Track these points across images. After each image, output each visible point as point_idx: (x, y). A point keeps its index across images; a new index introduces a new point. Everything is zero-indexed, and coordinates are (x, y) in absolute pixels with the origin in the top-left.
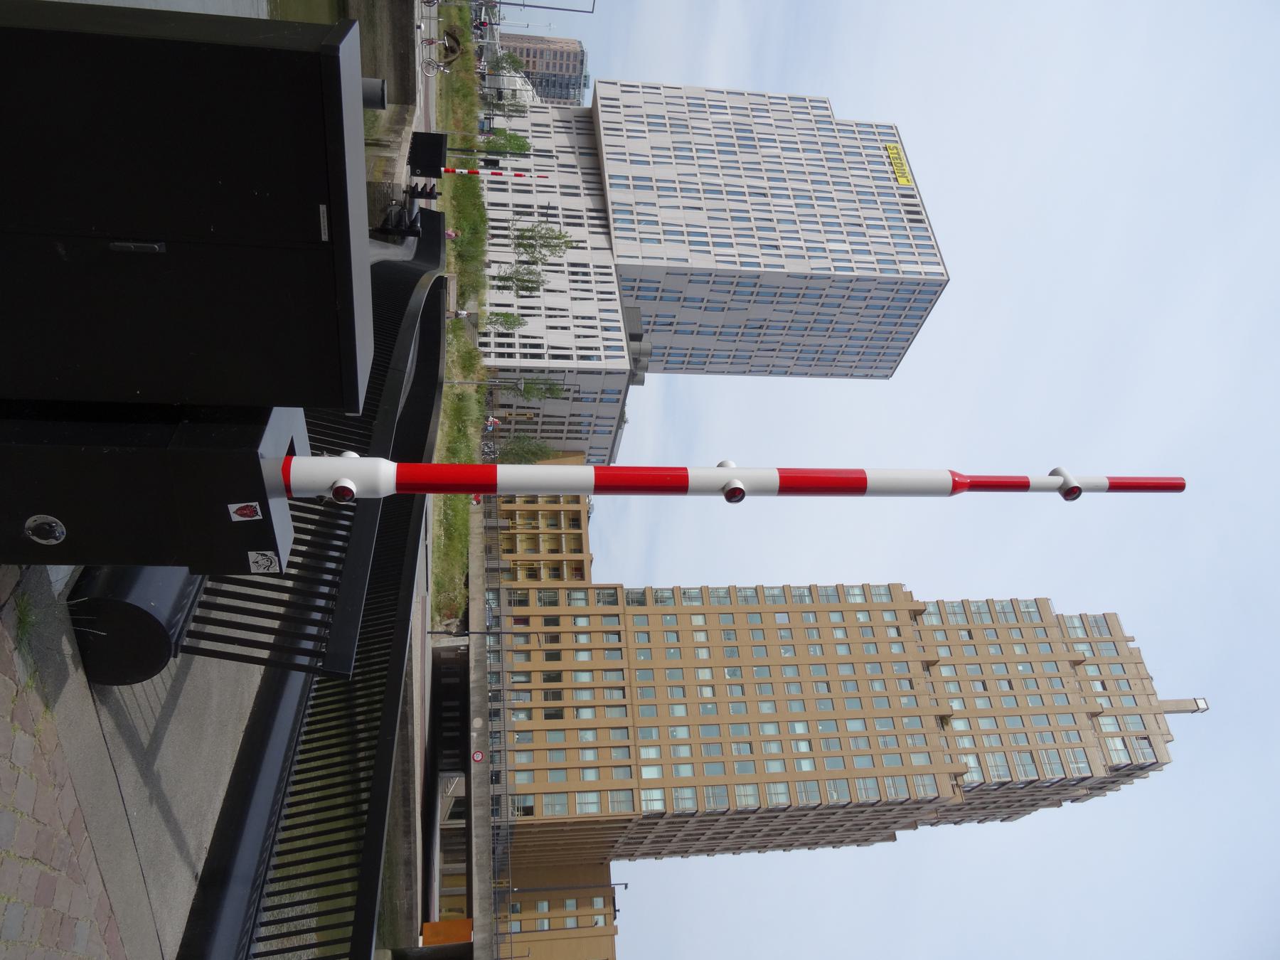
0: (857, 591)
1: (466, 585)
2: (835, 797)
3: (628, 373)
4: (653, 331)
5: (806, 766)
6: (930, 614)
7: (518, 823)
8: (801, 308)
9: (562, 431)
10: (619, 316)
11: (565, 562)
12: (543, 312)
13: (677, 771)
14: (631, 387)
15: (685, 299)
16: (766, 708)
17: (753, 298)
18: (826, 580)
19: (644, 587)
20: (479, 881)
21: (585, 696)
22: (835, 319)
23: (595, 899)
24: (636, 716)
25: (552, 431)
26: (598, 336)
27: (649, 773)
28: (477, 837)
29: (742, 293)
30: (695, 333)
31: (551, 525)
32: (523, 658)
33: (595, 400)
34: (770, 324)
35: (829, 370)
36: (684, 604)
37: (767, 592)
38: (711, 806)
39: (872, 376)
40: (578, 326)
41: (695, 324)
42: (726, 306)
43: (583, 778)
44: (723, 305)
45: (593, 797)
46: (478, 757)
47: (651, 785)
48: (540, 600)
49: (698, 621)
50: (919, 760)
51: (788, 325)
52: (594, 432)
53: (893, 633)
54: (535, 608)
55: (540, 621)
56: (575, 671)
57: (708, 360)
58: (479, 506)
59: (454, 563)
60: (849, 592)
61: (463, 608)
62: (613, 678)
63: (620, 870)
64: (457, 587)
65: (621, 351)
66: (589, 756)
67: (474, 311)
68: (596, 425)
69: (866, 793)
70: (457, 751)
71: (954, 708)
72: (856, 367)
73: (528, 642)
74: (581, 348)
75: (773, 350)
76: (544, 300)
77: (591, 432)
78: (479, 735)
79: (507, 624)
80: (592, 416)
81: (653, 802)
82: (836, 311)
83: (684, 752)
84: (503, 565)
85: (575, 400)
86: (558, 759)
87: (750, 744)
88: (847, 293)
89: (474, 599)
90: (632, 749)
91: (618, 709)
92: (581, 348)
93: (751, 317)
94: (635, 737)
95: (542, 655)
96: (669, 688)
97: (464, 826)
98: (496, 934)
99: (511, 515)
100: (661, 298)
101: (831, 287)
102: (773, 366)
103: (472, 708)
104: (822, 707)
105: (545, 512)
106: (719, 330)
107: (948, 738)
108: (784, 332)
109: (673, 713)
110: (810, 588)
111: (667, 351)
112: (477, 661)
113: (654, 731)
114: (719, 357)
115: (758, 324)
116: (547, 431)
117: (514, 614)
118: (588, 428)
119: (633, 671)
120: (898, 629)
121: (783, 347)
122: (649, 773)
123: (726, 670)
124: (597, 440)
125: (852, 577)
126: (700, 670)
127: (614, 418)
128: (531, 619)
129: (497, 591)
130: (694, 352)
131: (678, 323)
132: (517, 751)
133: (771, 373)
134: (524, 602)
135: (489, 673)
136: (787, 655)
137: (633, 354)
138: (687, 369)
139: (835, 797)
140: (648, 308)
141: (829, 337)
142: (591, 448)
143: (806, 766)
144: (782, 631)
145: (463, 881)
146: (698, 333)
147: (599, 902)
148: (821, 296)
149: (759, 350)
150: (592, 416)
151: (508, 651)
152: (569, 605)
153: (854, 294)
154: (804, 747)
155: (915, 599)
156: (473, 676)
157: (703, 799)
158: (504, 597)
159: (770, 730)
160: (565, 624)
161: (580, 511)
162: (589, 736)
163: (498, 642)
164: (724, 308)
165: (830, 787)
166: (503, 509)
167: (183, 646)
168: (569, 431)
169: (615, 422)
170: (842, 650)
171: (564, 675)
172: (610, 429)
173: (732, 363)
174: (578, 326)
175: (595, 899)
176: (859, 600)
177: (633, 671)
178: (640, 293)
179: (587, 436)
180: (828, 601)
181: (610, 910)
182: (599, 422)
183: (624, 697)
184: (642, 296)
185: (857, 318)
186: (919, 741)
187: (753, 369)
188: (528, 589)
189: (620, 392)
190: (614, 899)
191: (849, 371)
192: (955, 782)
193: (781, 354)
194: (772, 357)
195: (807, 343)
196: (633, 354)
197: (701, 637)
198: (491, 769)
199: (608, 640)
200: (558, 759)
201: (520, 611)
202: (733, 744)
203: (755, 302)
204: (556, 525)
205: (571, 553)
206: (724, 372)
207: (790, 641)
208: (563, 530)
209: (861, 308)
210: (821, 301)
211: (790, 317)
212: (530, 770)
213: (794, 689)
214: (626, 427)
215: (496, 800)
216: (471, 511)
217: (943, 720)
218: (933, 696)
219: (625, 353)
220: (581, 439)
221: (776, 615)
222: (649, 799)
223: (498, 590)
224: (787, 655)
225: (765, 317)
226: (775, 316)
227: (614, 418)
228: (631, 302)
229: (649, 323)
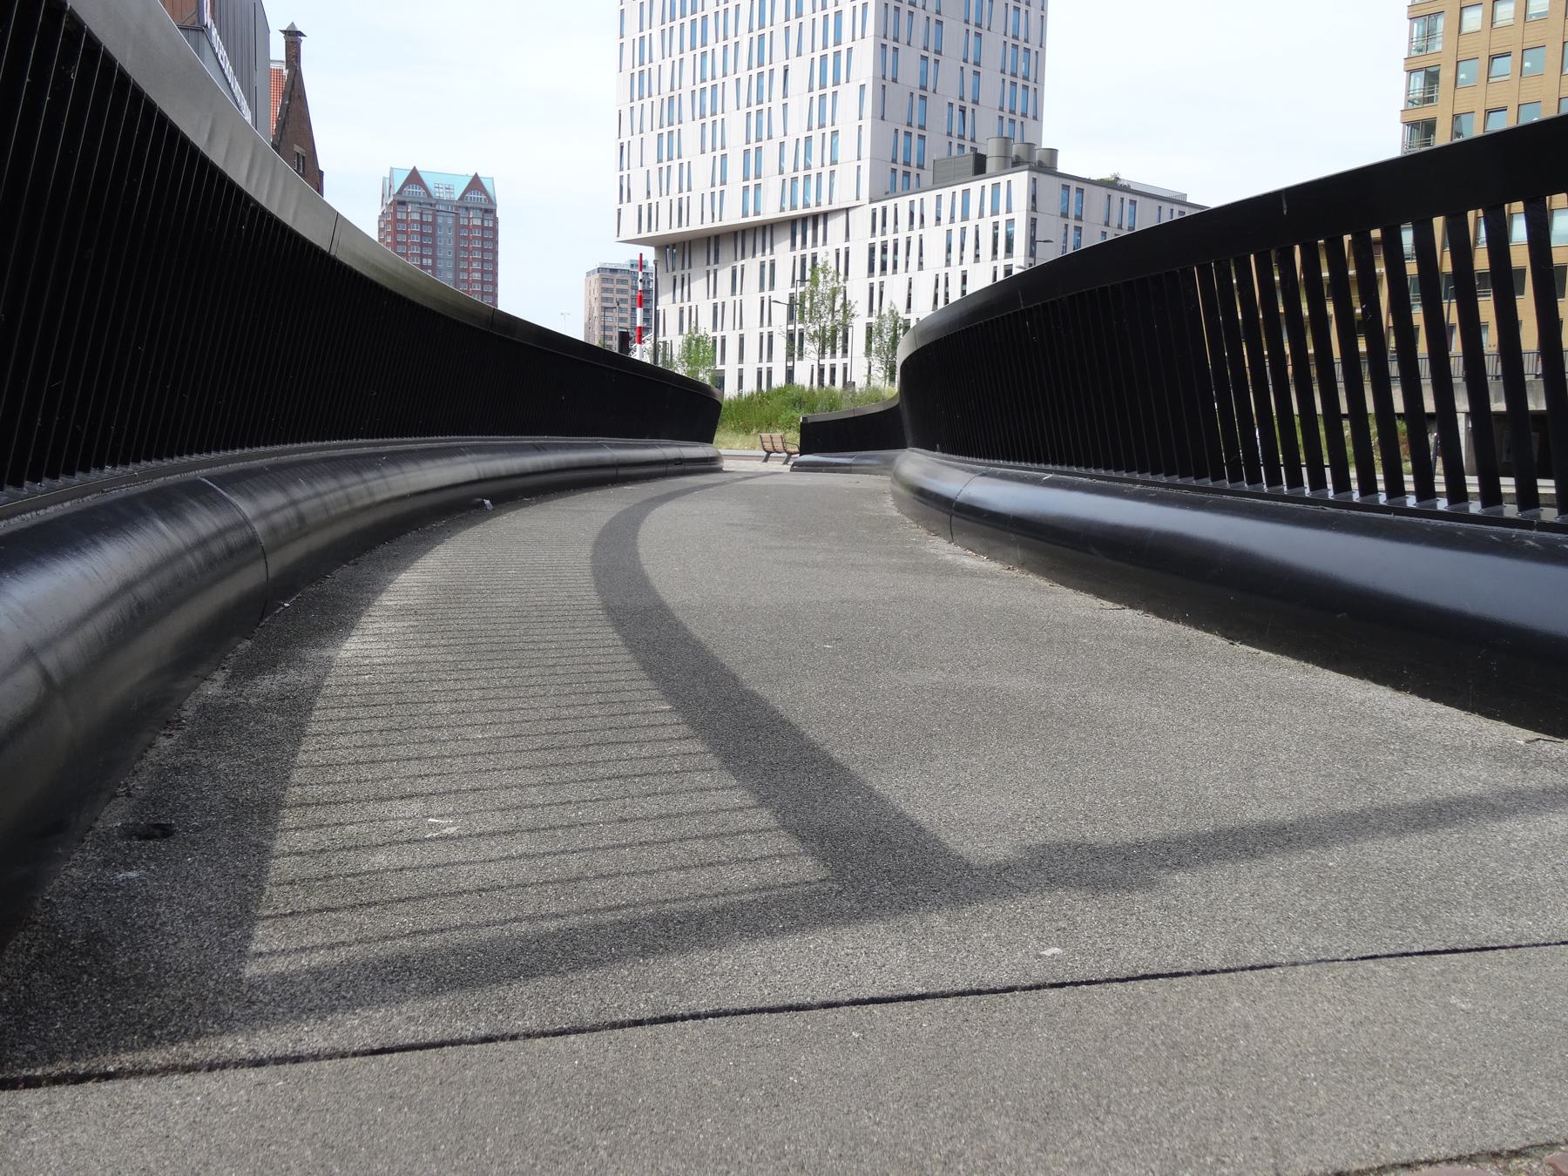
3: (1035, 175)
4: (973, 140)
10: (946, 193)
36: (1439, 47)
41: (962, 68)
42: (934, 17)
44: (932, 22)
57: (1022, 45)
74: (995, 252)
111: (1007, 116)
114: (1016, 27)
127: (1109, 196)
131: (962, 98)
137: (1005, 167)
138: (1036, 82)
140: (937, 147)
169: (1117, 195)
172: (1126, 202)
174: (962, 258)
178: (914, 162)
189: (1066, 188)
206: (1042, 17)
229: (961, 147)
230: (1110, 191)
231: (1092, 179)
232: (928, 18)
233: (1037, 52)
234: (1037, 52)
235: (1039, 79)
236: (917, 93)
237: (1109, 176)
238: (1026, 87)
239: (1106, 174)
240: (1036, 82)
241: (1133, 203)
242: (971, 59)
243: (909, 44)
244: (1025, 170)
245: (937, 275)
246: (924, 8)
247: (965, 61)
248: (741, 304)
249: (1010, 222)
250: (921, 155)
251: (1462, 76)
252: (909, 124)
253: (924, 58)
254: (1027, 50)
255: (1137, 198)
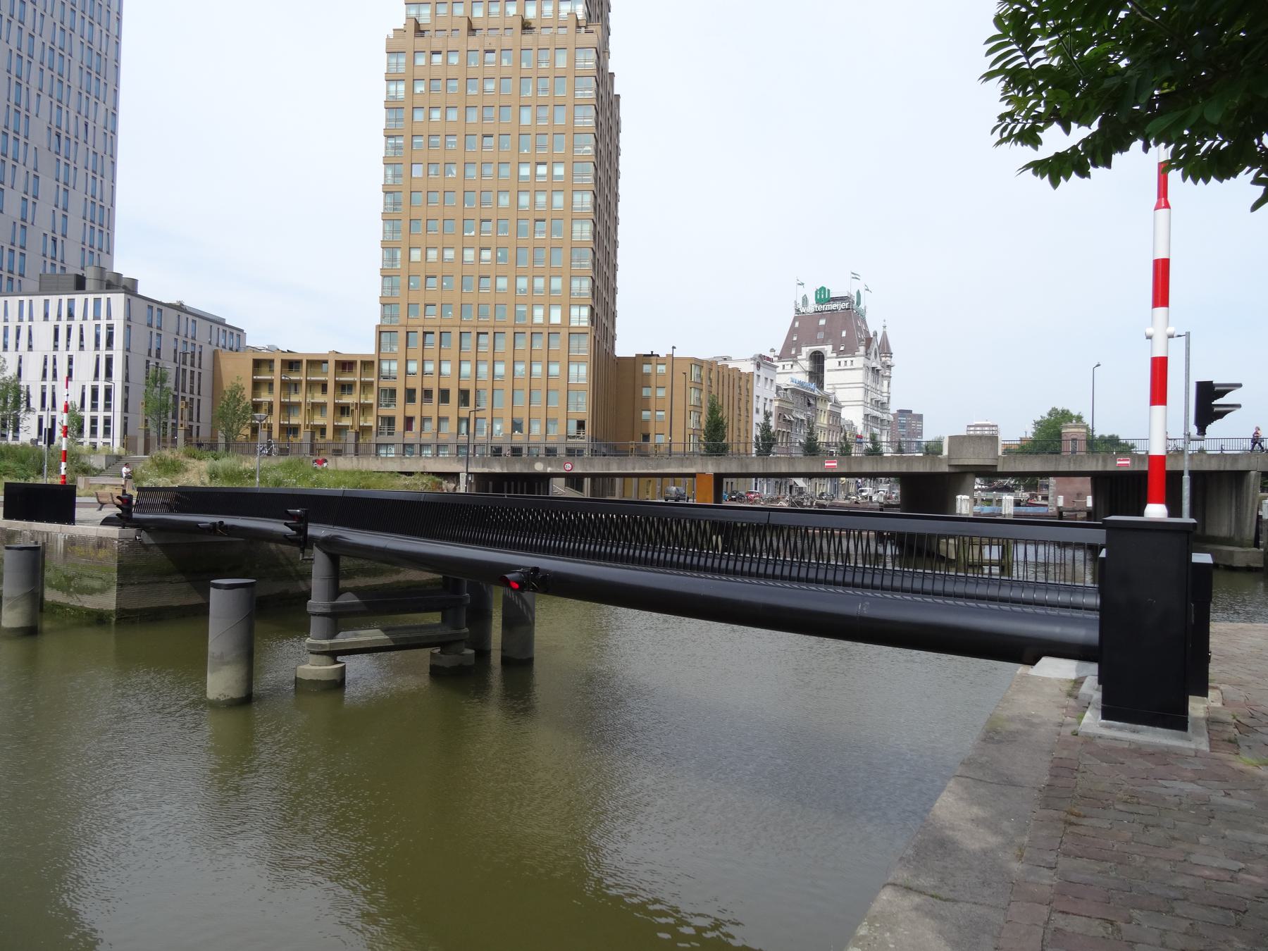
0: (393, 87)
1: (410, 474)
2: (589, 148)
3: (129, 297)
4: (62, 261)
5: (559, 171)
6: (419, 15)
7: (590, 434)
8: (34, 83)
9: (192, 372)
10: (53, 300)
11: (337, 379)
12: (49, 383)
13: (555, 291)
14: (140, 292)
15: (24, 220)
16: (505, 201)
17: (22, 140)
18: (378, 119)
19: (380, 305)
20: (669, 468)
21: (484, 369)
22: (48, 44)
23: (644, 372)
24: (504, 324)
25: (192, 382)
26: (81, 325)
27: (556, 317)
28: (634, 469)
29: (16, 152)
30: (65, 213)
31: (296, 391)
32: (445, 423)
33: (159, 335)
34: (54, 123)
35: (111, 64)
36: (399, 266)
37: (390, 182)
38: (588, 264)
39: (119, 13)
40: (68, 346)
41: (54, 211)
42: (32, 173)
43: (556, 376)
44: (31, 176)
45: (573, 368)
46: (568, 466)
47: (567, 316)
48: (388, 406)
49: (416, 255)
50: (562, 61)
51: (55, 103)
52: (194, 338)
53: (437, 59)
54: (398, 410)
55: (410, 406)
56: (459, 377)
57: (98, 203)
58: (329, 460)
59: (390, 485)
60: (393, 96)
61: (433, 477)
62: (469, 342)
63: (624, 349)
64: (414, 482)
65: (100, 301)
66: (537, 369)
67: (104, 459)
68: (186, 336)
69: (586, 119)
70: (536, 484)
71: (515, 13)
72: (108, 30)
73: (430, 419)
74: (97, 345)
75: (86, 125)
76: (32, 380)
77: (193, 342)
78: (550, 465)
79: (411, 437)
80: (176, 340)
81: (580, 316)
82: (38, 41)
83: (539, 283)
84: (308, 440)
85: (158, 356)
86: (539, 397)
87: (537, 220)
88: (15, 24)
89: (424, 466)
90: (534, 330)
91: (497, 341)
92: (97, 345)
93: (45, 145)
94: (524, 326)
95: (443, 407)
96: (481, 291)
97: (589, 479)
98: (670, 455)
99: (339, 430)
100: (23, 247)
101: (7, 42)
102: (106, 128)
103: (525, 471)
104: (506, 145)
105: (282, 394)
106: (62, 186)
107: (543, 26)
108: (64, 109)
109: (504, 290)
110: (387, 137)
111: (88, 249)
112: (483, 467)
113: (520, 308)
114: (94, 189)
115: (54, 138)
116: (192, 387)
117: (402, 430)
118: (189, 345)
119: (463, 323)
120: (434, 53)
121: (83, 112)
122: (556, 317)
123: (466, 234)
124: (202, 338)
125: (378, 91)
126: (465, 260)
127: (179, 316)
128: (407, 414)
129: (378, 446)
130: (88, 218)
131: (54, 232)
132: (529, 433)
133: (114, 132)
134: (390, 421)
135: (457, 455)
136: (454, 172)
137: (101, 288)
138: (108, 229)
139: (589, 148)
140: (34, 265)
141: (70, 55)
142: (210, 343)
143: (559, 171)
144: (430, 173)
145: (628, 480)
146: (65, 210)
147: (647, 368)
148: (20, 57)
149: (86, 142)
150: (176, 340)
151: (437, 437)
152: (395, 379)
153: (16, 15)
154: (542, 170)
155: (402, 27)
156: (497, 470)
157: (581, 271)
158: (384, 439)
159: (525, 200)
160: (414, 383)
161: (282, 360)
162: (520, 368)
163: (428, 445)
164: (35, 176)
165: (579, 152)
166: (278, 437)
167: (1171, 515)
168: (192, 365)
169: (183, 316)
170: (453, 115)
171: (463, 387)
172: (190, 321)
173: (102, 176)
174: (68, 346)
175: (644, 372)
176: (401, 87)
177: (463, 323)
178: (16, 271)
179: (197, 346)
180: (402, 120)
181: (653, 359)
182: (182, 332)
183: (487, 333)
184: (9, 266)
185: (47, 16)
186: (545, 56)
187: (109, 152)
188: (378, 416)
189: (151, 307)
190: (645, 355)
191: (112, 40)
192: (583, 29)
193: (91, 116)
194: (95, 127)
195: (78, 84)
196: (101, 288)
197: (433, 255)
198: (544, 456)
199: (432, 344)
200: (539, 397)
201: (399, 425)
202: (536, 237)
203: (26, 137)
204: (296, 385)
205: (273, 371)
206: (113, 187)
207: (440, 167)
208: (303, 378)
209: (35, 10)
210: (26, 58)
211: (45, 99)
212: (492, 420)
213: (488, 171)
214: (188, 303)
215: (571, 452)
216: (335, 469)
217: (526, 26)
218: (501, 31)
219: (104, 297)
220: (200, 353)
221: (413, 176)
222: (578, 319)
223: (378, 445)
224: (454, 172)
225: (45, 130)
226: (45, 116)
227: (179, 316)
228: (31, 283)
229: (53, 265)
230: (179, 313)
231: (163, 302)
232: (28, 172)
233: (109, 209)
234: (109, 209)
235: (110, 227)
236: (19, 223)
237: (175, 302)
238: (101, 231)
239: (173, 301)
240: (108, 229)
241: (194, 321)
242: (61, 206)
243: (12, 187)
244: (122, 292)
245: (46, 356)
246: (24, 165)
247: (56, 206)
248: (54, 394)
249: (110, 327)
250: (22, 267)
251: (412, 284)
252: (13, 244)
253: (24, 199)
254: (102, 207)
255: (197, 319)
